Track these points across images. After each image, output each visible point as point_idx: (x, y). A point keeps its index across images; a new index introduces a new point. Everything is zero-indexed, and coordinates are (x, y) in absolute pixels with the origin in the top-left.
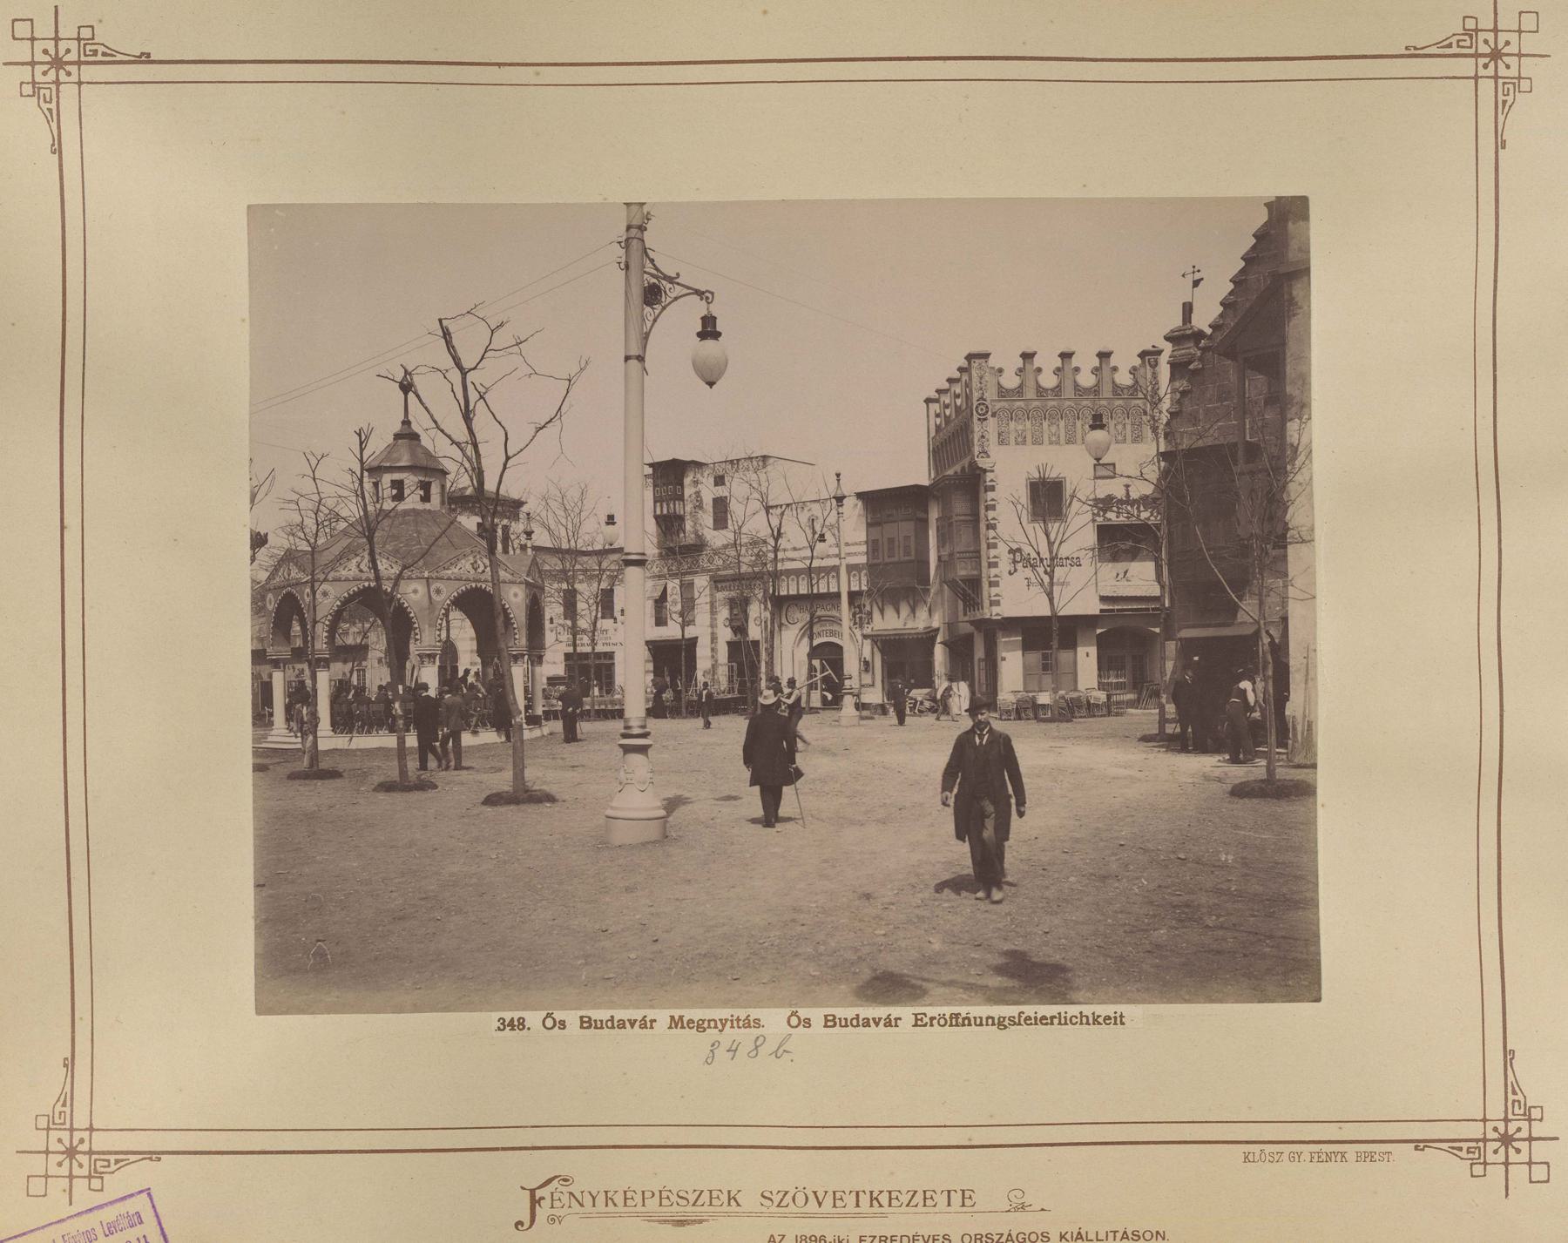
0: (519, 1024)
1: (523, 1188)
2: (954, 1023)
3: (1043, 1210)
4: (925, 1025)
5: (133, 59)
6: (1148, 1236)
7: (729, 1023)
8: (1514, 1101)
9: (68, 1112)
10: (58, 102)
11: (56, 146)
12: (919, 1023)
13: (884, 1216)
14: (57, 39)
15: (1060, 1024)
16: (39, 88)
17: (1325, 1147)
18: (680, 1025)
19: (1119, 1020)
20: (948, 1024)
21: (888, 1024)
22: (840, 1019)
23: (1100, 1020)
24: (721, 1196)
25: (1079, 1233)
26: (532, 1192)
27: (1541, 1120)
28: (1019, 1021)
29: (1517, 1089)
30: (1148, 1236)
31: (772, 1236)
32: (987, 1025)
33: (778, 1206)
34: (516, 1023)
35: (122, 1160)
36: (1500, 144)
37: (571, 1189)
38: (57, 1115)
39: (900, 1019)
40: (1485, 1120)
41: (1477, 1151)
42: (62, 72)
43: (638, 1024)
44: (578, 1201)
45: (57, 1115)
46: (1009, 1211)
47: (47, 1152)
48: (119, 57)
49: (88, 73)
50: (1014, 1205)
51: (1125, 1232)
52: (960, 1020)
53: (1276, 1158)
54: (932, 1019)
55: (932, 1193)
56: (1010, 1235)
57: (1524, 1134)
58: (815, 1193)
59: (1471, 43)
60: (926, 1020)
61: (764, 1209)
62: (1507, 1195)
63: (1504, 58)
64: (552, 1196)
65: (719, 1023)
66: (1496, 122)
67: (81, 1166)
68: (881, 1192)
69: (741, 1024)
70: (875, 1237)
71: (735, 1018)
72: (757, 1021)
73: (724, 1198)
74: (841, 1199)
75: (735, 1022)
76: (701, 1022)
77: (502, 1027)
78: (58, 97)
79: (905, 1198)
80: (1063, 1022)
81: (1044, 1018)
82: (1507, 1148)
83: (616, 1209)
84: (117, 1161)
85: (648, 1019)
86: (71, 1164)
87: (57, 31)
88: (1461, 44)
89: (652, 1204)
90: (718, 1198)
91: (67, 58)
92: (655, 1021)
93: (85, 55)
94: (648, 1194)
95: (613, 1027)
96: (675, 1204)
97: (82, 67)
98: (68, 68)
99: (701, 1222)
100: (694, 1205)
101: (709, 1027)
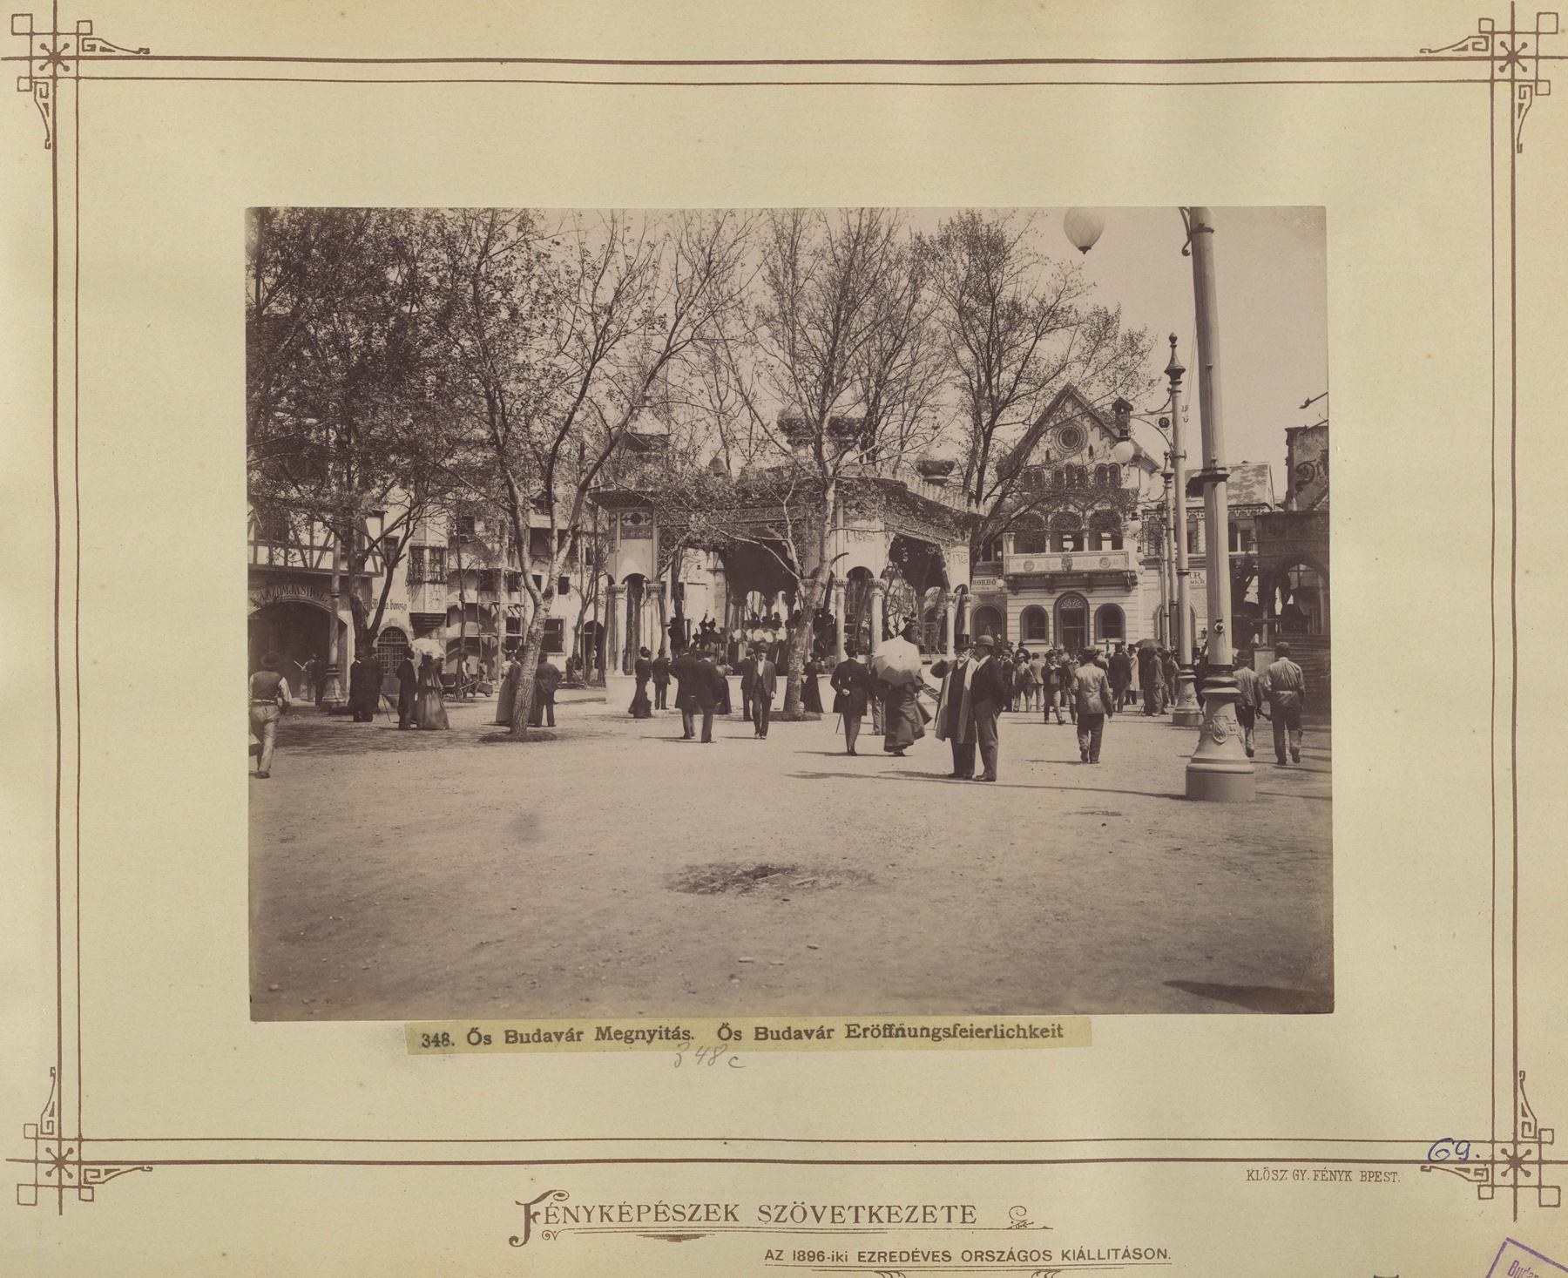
0: (444, 1039)
3: (1045, 1228)
4: (858, 1036)
6: (1149, 1254)
7: (657, 1035)
8: (1524, 1123)
10: (54, 97)
11: (51, 141)
12: (852, 1034)
13: (882, 1231)
15: (996, 1036)
16: (36, 83)
17: (1330, 1166)
18: (607, 1037)
19: (1058, 1032)
21: (821, 1035)
22: (772, 1032)
23: (1038, 1032)
24: (718, 1210)
25: (1081, 1252)
26: (527, 1207)
27: (1552, 1143)
28: (955, 1032)
30: (1149, 1254)
31: (769, 1251)
32: (922, 1036)
33: (776, 1221)
34: (440, 1039)
36: (1517, 148)
38: (45, 1124)
39: (833, 1030)
40: (1493, 1142)
41: (1485, 1173)
43: (564, 1036)
45: (45, 1124)
46: (1011, 1228)
47: (36, 1161)
48: (118, 53)
49: (87, 68)
50: (1016, 1223)
51: (1127, 1250)
52: (894, 1031)
53: (1280, 1175)
54: (865, 1030)
55: (932, 1209)
57: (37, 64)
58: (813, 1208)
59: (1487, 46)
60: (859, 1031)
62: (1515, 1219)
63: (1521, 61)
67: (70, 1176)
68: (881, 1207)
69: (670, 1035)
70: (874, 1253)
72: (687, 1033)
73: (722, 1212)
74: (840, 1214)
75: (664, 1035)
77: (426, 1043)
78: (55, 92)
79: (905, 1214)
80: (999, 1034)
81: (980, 1030)
82: (1516, 1171)
86: (60, 1174)
87: (55, 27)
88: (1476, 46)
90: (715, 1212)
91: (64, 53)
92: (582, 1033)
93: (84, 50)
94: (644, 1209)
95: (539, 1041)
96: (671, 1219)
97: (81, 61)
98: (66, 63)
99: (697, 1237)
100: (690, 1219)
101: (637, 1038)
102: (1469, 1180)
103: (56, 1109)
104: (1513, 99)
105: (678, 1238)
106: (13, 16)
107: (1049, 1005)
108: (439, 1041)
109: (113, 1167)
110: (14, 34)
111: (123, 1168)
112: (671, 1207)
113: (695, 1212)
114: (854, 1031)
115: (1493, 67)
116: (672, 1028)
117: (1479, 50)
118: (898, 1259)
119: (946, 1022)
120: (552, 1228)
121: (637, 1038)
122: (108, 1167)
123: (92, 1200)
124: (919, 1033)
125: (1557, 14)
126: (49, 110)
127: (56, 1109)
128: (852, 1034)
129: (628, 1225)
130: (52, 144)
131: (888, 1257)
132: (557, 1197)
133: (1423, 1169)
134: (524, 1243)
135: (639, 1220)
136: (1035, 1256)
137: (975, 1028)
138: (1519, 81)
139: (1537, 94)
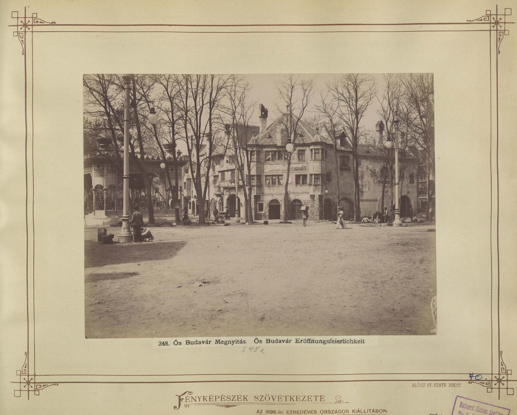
1: (176, 395)
2: (309, 342)
3: (347, 402)
4: (299, 342)
5: (49, 24)
6: (381, 411)
7: (235, 342)
8: (502, 368)
9: (27, 371)
10: (25, 38)
11: (24, 52)
14: (25, 18)
15: (343, 343)
16: (19, 34)
18: (219, 343)
19: (363, 342)
20: (307, 342)
21: (287, 342)
22: (271, 340)
23: (357, 342)
25: (358, 410)
26: (179, 397)
27: (511, 374)
29: (45, 386)
30: (381, 411)
32: (320, 343)
33: (260, 400)
34: (165, 343)
35: (502, 364)
37: (192, 396)
42: (27, 28)
43: (205, 342)
44: (193, 398)
47: (20, 383)
48: (45, 23)
49: (35, 28)
50: (337, 401)
51: (373, 410)
52: (311, 341)
53: (423, 385)
54: (301, 341)
56: (336, 411)
57: (505, 379)
60: (300, 341)
61: (255, 402)
62: (499, 399)
63: (499, 24)
64: (186, 398)
65: (232, 342)
66: (497, 45)
67: (32, 387)
69: (239, 342)
71: (237, 340)
73: (242, 398)
75: (237, 342)
76: (226, 342)
77: (160, 345)
78: (25, 36)
79: (302, 398)
80: (344, 342)
83: (207, 402)
84: (44, 386)
85: (208, 341)
86: (28, 386)
87: (25, 15)
88: (485, 19)
89: (219, 400)
93: (34, 23)
94: (217, 397)
95: (197, 344)
97: (33, 26)
98: (29, 27)
99: (234, 406)
100: (232, 400)
101: (229, 343)
102: (485, 386)
103: (27, 366)
104: (497, 36)
105: (228, 406)
106: (12, 12)
107: (360, 332)
108: (165, 344)
109: (45, 384)
110: (12, 18)
111: (49, 384)
112: (226, 396)
113: (234, 398)
114: (298, 341)
115: (490, 26)
116: (239, 340)
117: (486, 20)
118: (299, 413)
119: (328, 338)
120: (188, 403)
121: (229, 343)
122: (481, 22)
123: (39, 395)
124: (319, 342)
125: (511, 9)
126: (24, 42)
127: (27, 366)
128: (297, 341)
129: (212, 402)
130: (24, 53)
131: (296, 412)
132: (189, 393)
133: (469, 383)
134: (179, 408)
135: (216, 401)
136: (344, 412)
137: (337, 340)
138: (499, 30)
139: (505, 35)
